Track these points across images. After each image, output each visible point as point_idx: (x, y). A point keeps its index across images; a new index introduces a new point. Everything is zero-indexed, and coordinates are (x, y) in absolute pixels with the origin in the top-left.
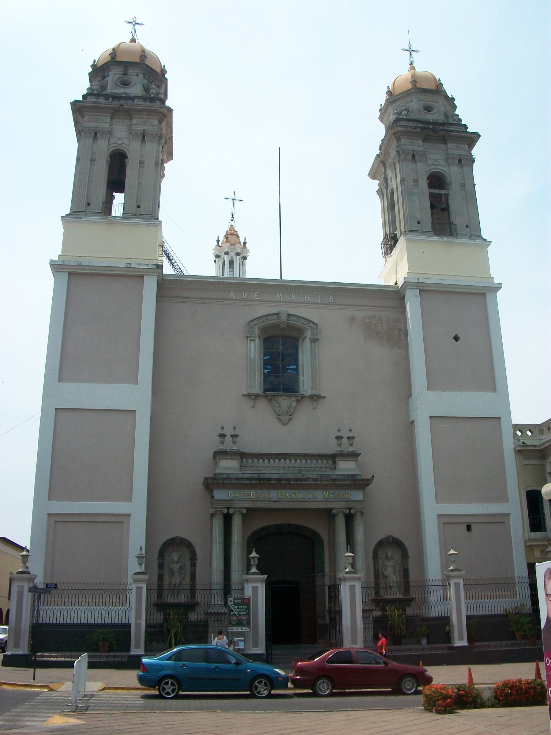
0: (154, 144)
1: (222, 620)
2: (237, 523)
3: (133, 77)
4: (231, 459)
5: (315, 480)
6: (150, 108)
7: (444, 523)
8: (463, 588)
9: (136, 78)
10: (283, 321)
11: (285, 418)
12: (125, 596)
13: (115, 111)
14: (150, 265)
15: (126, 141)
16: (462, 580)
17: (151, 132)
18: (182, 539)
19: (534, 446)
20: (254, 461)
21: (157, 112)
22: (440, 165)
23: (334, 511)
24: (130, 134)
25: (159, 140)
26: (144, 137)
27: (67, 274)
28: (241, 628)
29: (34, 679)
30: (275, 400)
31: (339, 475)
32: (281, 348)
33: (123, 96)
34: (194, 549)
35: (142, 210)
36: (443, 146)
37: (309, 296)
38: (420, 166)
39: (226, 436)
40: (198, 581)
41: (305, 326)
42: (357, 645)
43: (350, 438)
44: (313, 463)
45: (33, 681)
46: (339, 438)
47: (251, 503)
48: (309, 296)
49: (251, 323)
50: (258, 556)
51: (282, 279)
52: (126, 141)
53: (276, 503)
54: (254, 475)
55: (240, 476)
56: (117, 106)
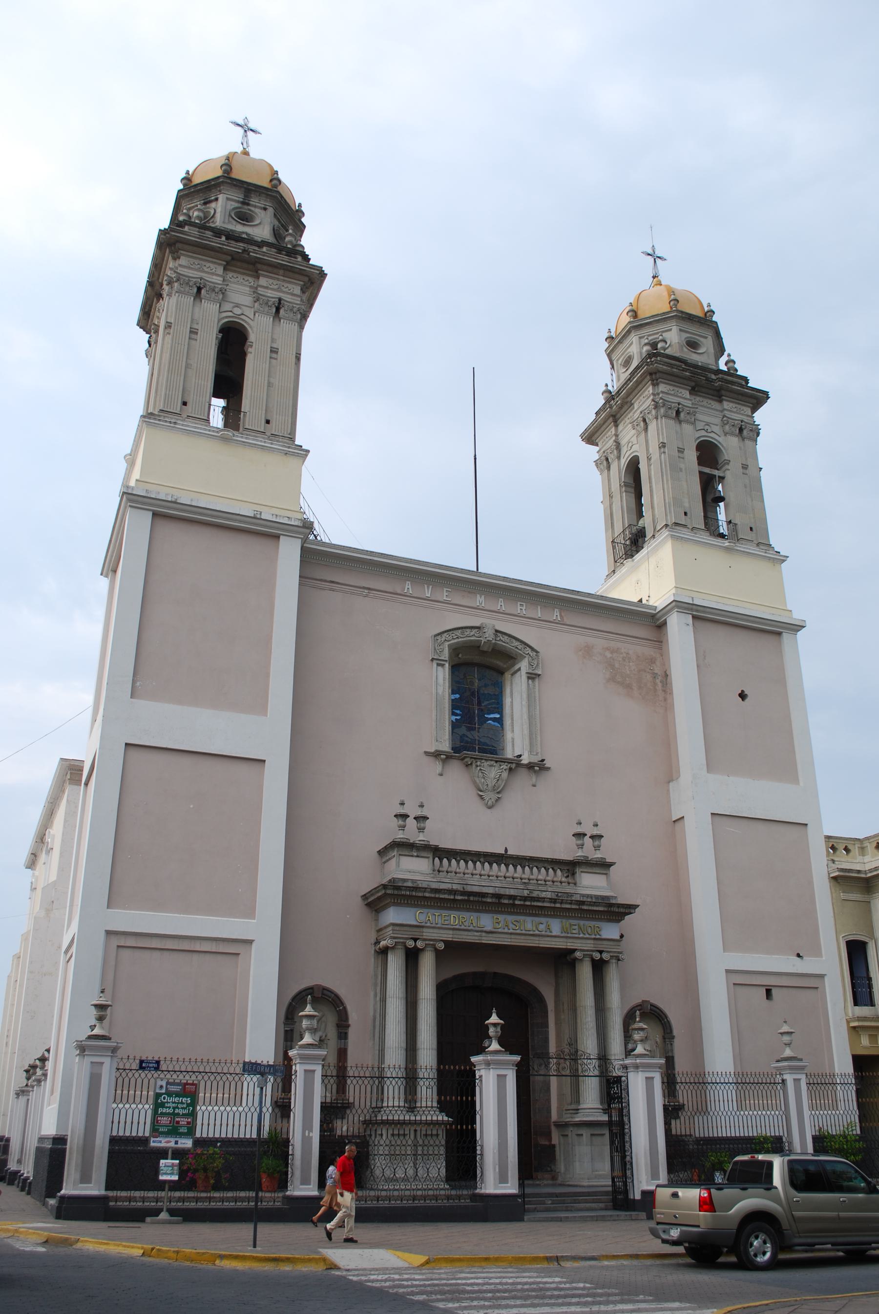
1: (407, 1134)
4: (417, 856)
6: (291, 265)
7: (734, 984)
9: (263, 212)
11: (490, 796)
12: (239, 1084)
13: (233, 259)
15: (249, 312)
18: (325, 989)
19: (859, 872)
21: (301, 272)
23: (578, 954)
24: (255, 302)
25: (301, 320)
26: (278, 309)
27: (151, 514)
28: (176, 1146)
31: (583, 895)
34: (345, 1009)
35: (273, 428)
36: (715, 405)
37: (524, 606)
38: (687, 428)
39: (409, 816)
40: (351, 1061)
41: (520, 652)
42: (659, 1180)
43: (596, 837)
44: (542, 874)
46: (580, 835)
47: (451, 932)
48: (524, 606)
50: (502, 1022)
51: (479, 571)
52: (249, 312)
53: (490, 935)
54: (455, 887)
55: (434, 886)
56: (240, 251)
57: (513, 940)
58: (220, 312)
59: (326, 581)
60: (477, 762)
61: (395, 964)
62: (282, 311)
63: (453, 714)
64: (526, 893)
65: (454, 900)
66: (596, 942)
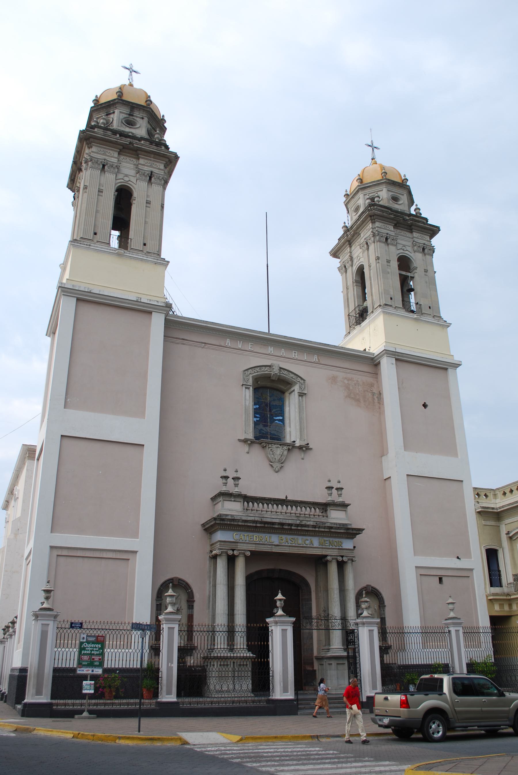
0: (160, 187)
1: (229, 665)
2: (240, 565)
3: (138, 119)
4: (234, 501)
5: (314, 526)
8: (177, 634)
9: (141, 120)
10: (275, 374)
11: (277, 465)
12: (130, 636)
13: (124, 148)
14: (160, 302)
15: (134, 180)
16: (177, 625)
17: (158, 175)
19: (493, 508)
20: (264, 506)
21: (164, 156)
22: (407, 250)
23: (329, 558)
24: (137, 173)
26: (150, 178)
27: (75, 299)
29: (139, 731)
30: (269, 448)
31: (332, 523)
32: (269, 398)
33: (129, 135)
34: (192, 591)
35: (148, 248)
36: (409, 234)
37: (297, 353)
38: (392, 248)
39: (229, 477)
40: (195, 622)
42: (377, 690)
43: (339, 489)
45: (137, 733)
46: (330, 488)
47: (254, 545)
48: (297, 353)
49: (246, 372)
50: (284, 598)
51: (270, 332)
52: (134, 180)
53: (277, 547)
55: (244, 518)
56: (128, 143)
57: (290, 550)
58: (116, 180)
59: (179, 339)
60: (269, 445)
61: (221, 565)
62: (153, 179)
63: (255, 417)
64: (298, 522)
65: (256, 527)
66: (339, 551)
